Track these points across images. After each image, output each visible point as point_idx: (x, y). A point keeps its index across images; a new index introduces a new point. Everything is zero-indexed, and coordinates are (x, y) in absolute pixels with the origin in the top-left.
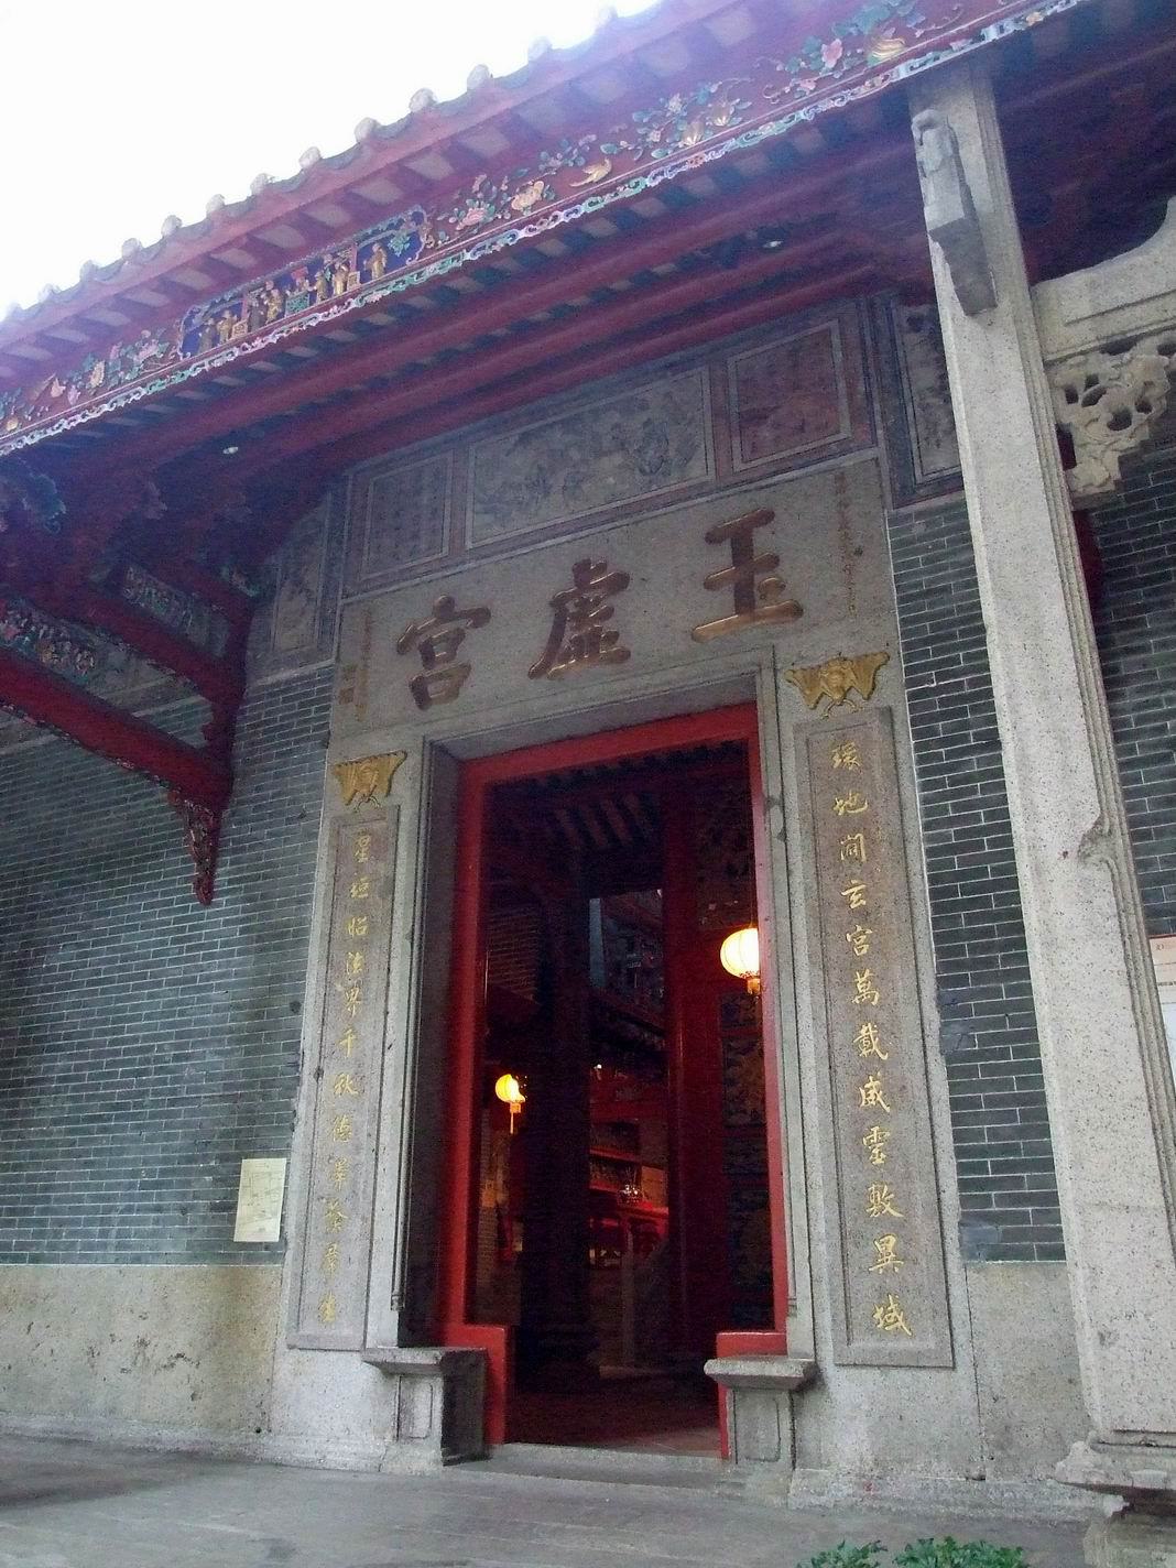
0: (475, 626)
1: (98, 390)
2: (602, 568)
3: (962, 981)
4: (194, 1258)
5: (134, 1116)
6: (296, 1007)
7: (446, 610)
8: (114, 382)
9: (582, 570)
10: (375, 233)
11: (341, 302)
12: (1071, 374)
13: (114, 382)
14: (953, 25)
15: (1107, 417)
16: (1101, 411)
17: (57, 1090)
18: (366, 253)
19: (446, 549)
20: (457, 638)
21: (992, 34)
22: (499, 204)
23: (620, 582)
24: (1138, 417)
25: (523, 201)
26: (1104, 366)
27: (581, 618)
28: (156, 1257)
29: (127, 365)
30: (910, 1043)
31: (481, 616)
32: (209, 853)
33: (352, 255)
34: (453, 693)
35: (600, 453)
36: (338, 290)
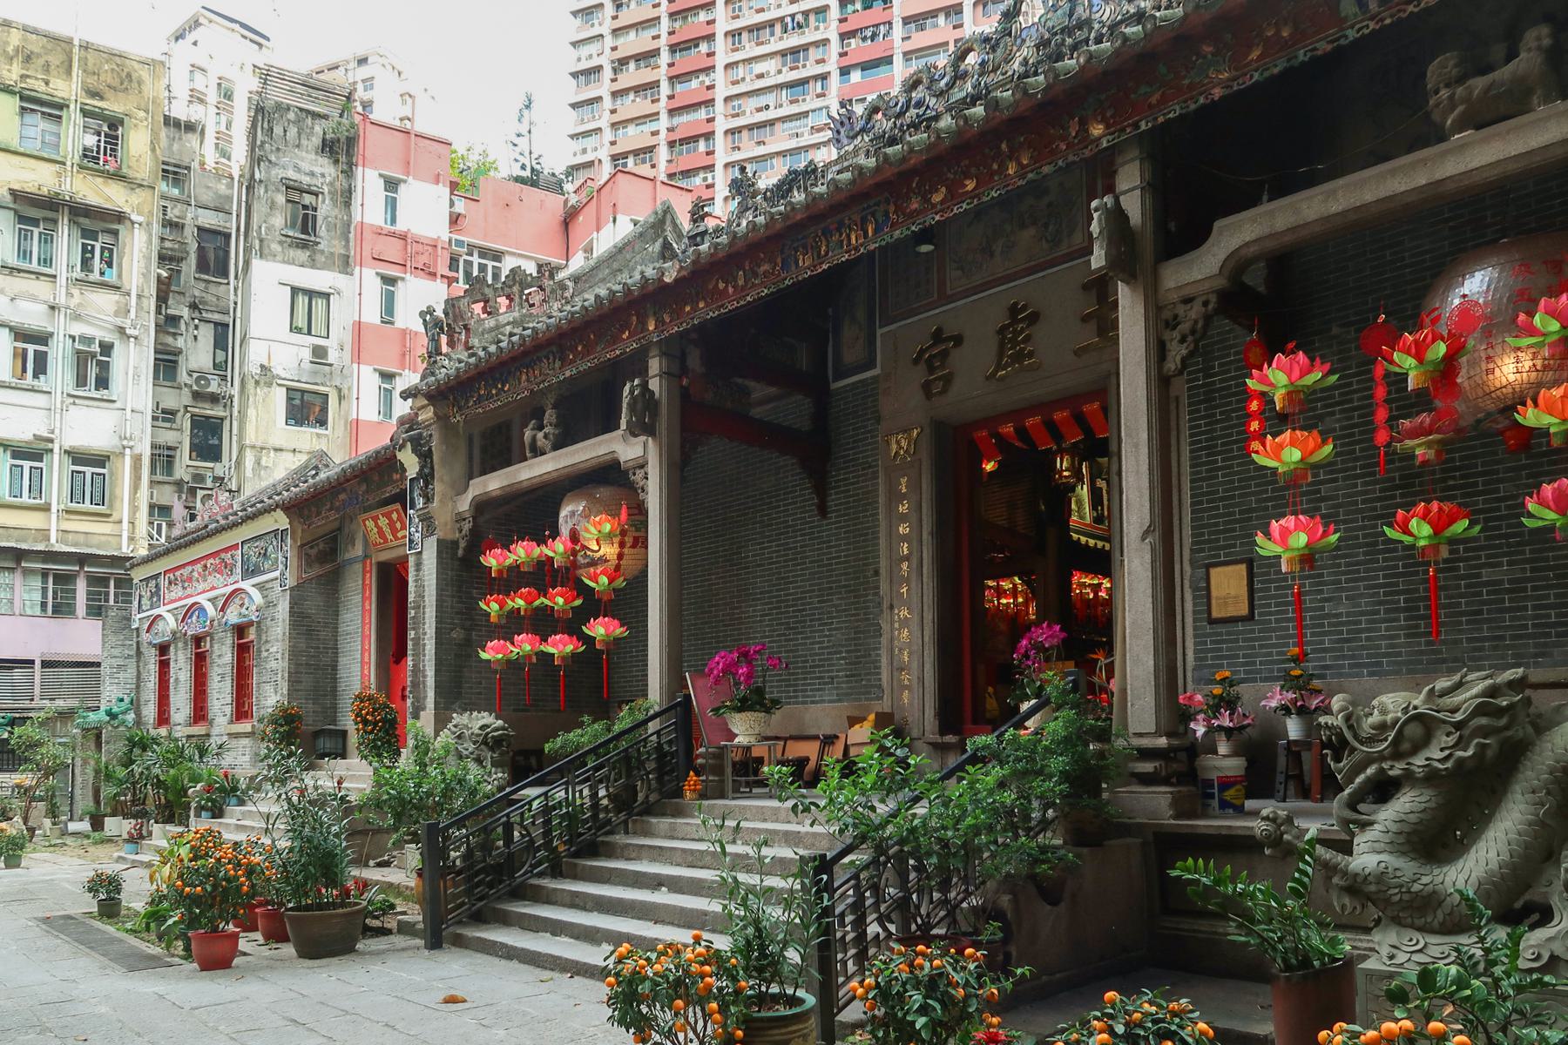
0: (954, 346)
1: (743, 288)
2: (1025, 308)
3: (1202, 550)
4: (839, 701)
5: (802, 633)
6: (877, 573)
7: (938, 336)
8: (750, 285)
9: (1014, 310)
10: (869, 207)
11: (856, 249)
12: (1167, 314)
13: (750, 285)
14: (1125, 120)
15: (1179, 338)
16: (1176, 334)
17: (761, 621)
18: (864, 221)
19: (936, 295)
20: (944, 354)
21: (1143, 126)
22: (926, 200)
23: (1034, 318)
24: (1190, 338)
25: (937, 198)
26: (1181, 310)
27: (1014, 342)
28: (823, 701)
29: (756, 275)
30: (900, 650)
31: (958, 340)
32: (821, 490)
33: (857, 218)
34: (944, 391)
35: (1023, 226)
36: (853, 241)
